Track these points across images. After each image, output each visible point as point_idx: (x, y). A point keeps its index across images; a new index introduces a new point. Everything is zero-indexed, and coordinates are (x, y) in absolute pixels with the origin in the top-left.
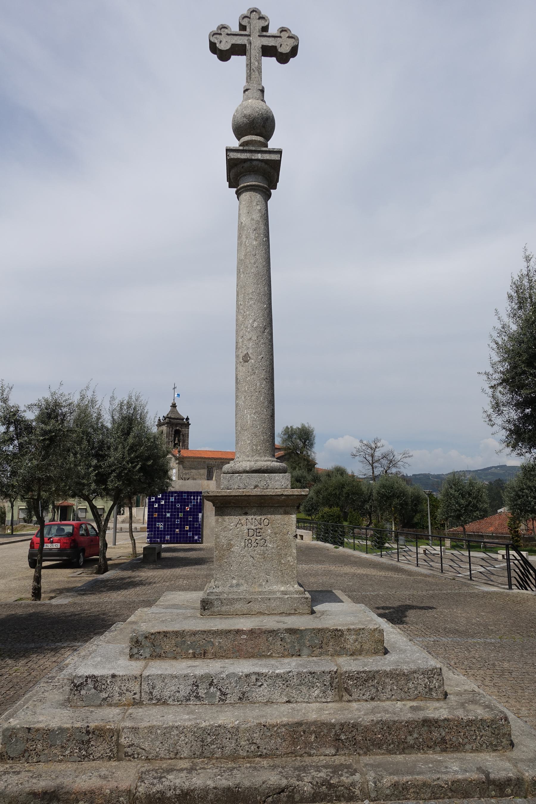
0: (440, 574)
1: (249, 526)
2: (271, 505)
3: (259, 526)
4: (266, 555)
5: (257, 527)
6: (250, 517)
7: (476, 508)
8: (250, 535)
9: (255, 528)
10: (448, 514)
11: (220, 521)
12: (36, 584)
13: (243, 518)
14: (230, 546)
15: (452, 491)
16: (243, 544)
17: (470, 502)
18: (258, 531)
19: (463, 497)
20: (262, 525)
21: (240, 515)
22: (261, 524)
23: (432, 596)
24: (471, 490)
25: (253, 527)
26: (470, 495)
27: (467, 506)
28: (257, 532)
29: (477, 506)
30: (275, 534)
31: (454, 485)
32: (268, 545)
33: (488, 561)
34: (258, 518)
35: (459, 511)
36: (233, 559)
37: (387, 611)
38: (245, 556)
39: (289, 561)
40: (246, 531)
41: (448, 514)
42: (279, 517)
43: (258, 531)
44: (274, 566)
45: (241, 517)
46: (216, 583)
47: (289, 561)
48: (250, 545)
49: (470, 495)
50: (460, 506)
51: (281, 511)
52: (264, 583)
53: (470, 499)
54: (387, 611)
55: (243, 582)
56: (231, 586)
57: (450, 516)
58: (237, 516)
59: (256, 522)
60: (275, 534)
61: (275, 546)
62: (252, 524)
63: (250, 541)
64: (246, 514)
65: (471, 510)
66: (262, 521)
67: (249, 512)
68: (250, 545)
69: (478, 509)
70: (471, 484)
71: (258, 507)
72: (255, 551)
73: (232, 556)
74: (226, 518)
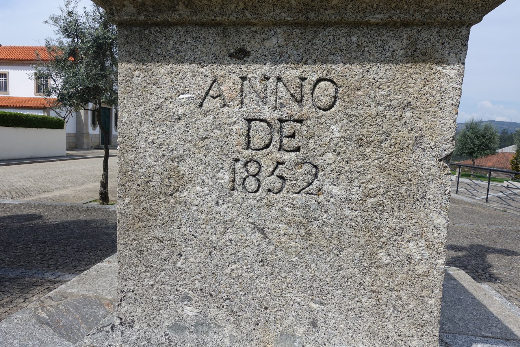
0: (484, 204)
1: (253, 107)
2: (350, 16)
3: (294, 110)
4: (314, 227)
5: (284, 113)
6: (255, 70)
7: (487, 147)
8: (255, 142)
9: (277, 114)
10: (462, 150)
11: (136, 81)
12: (103, 189)
13: (229, 73)
14: (175, 182)
15: (469, 134)
16: (225, 177)
17: (483, 142)
18: (288, 127)
19: (478, 138)
20: (308, 104)
21: (217, 60)
22: (300, 102)
23: (500, 233)
24: (485, 134)
25: (267, 112)
26: (484, 137)
27: (480, 145)
28: (285, 131)
29: (488, 146)
30: (361, 143)
31: (472, 129)
32: (328, 187)
33: (472, 186)
34: (291, 74)
35: (473, 149)
36: (186, 230)
37: (460, 254)
38: (232, 223)
39: (409, 257)
40: (240, 127)
41: (462, 150)
42: (381, 71)
43: (288, 127)
44: (347, 273)
45: (219, 71)
46: (125, 308)
47: (409, 257)
48: (251, 184)
49: (484, 137)
50: (474, 145)
51: (397, 44)
52: (300, 331)
53: (483, 140)
54: (460, 254)
55: (222, 315)
56: (178, 327)
57: (464, 153)
58: (203, 63)
59: (283, 93)
60: (361, 143)
61: (357, 192)
62: (264, 100)
63: (253, 168)
64: (241, 55)
65: (483, 149)
66: (307, 88)
67: (253, 47)
68: (251, 184)
69: (489, 148)
70: (486, 129)
71: (295, 24)
72: (270, 206)
73: (184, 218)
74: (162, 70)
